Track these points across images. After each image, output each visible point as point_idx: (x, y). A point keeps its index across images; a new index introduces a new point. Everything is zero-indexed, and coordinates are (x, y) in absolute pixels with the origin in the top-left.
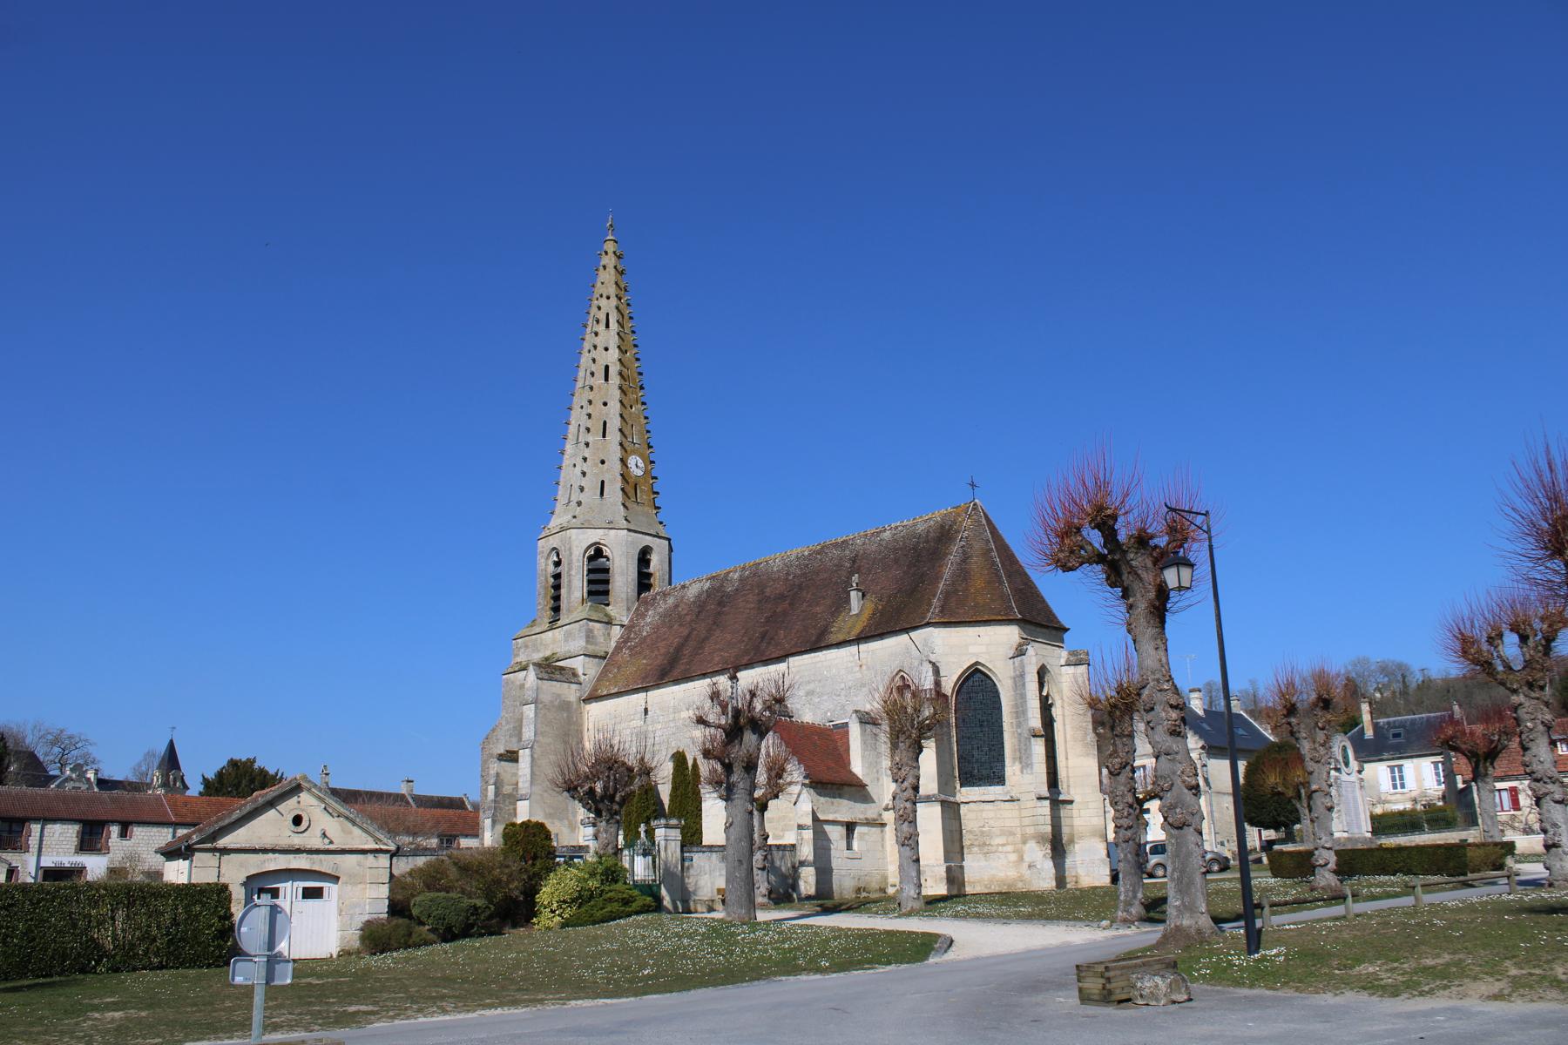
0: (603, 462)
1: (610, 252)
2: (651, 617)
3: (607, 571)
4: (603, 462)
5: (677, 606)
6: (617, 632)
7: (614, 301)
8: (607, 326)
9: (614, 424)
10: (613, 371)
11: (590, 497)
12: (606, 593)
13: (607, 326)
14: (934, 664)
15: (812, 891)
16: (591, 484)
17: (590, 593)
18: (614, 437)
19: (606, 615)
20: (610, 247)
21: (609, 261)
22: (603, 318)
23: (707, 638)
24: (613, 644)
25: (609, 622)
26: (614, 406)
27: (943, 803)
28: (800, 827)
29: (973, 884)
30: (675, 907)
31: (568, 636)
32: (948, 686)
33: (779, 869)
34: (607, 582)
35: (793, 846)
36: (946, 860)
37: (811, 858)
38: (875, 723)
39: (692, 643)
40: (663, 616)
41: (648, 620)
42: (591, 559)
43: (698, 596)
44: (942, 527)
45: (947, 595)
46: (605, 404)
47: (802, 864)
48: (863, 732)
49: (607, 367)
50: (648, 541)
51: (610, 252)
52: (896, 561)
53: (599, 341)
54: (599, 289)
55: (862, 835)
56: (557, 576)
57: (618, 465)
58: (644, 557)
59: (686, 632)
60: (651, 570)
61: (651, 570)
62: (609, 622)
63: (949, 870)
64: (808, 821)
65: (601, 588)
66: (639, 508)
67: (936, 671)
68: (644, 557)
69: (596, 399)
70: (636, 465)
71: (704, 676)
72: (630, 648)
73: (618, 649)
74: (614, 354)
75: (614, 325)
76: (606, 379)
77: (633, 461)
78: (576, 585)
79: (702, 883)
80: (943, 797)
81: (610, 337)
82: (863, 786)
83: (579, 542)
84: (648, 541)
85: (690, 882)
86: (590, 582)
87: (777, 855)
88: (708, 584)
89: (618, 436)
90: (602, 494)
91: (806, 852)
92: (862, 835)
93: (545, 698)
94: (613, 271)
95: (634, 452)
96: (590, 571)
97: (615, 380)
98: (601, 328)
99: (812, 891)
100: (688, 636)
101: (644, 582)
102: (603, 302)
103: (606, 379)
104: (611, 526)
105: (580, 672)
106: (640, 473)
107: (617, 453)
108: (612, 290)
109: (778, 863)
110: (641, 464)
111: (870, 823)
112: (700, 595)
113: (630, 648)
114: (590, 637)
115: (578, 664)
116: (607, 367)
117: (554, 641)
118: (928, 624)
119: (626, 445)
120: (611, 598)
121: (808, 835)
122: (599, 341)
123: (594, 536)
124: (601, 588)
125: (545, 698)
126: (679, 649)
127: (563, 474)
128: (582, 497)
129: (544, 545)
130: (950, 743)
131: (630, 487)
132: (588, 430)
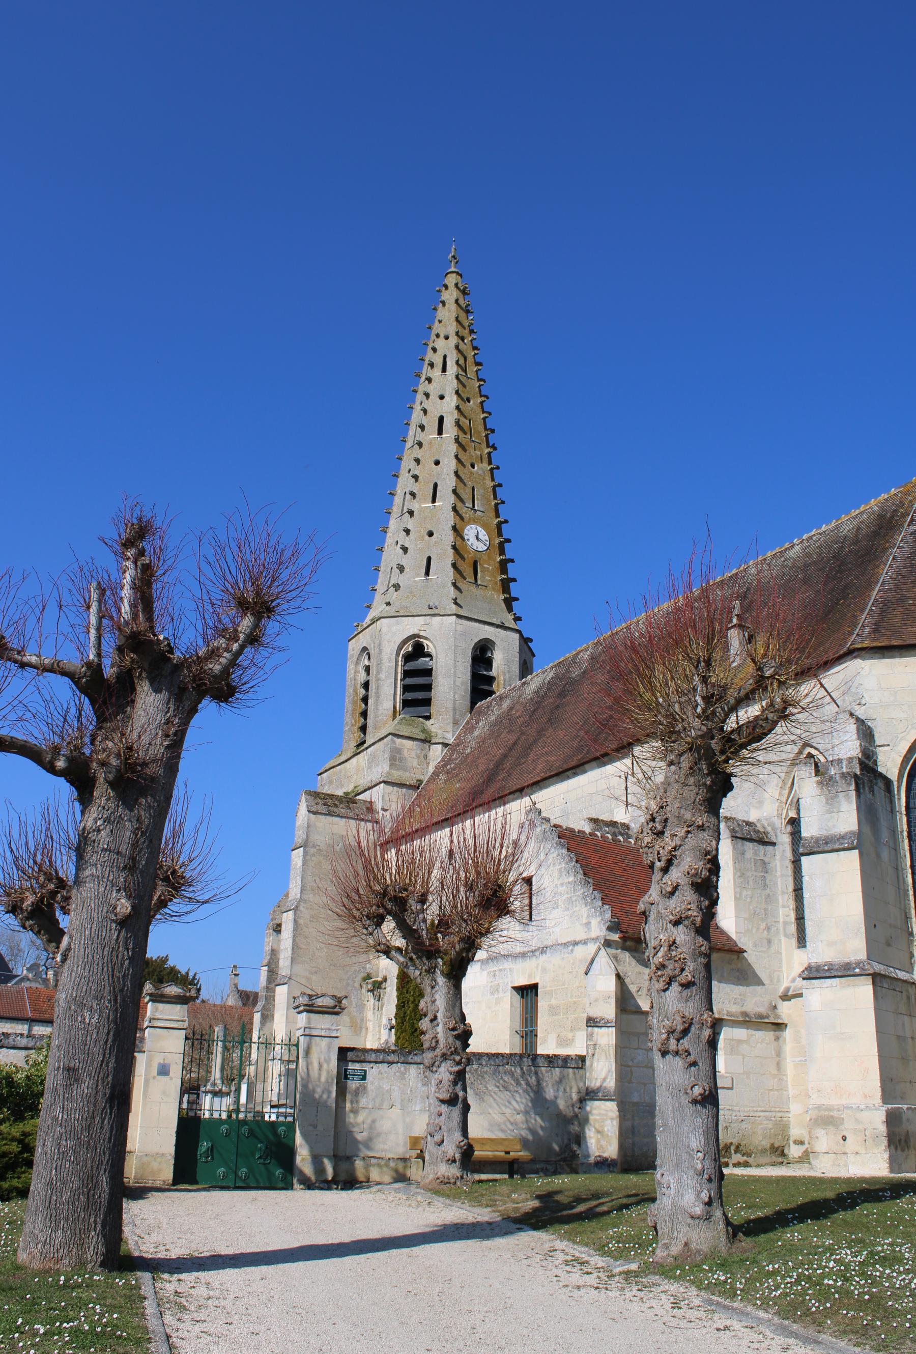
0: (431, 534)
1: (451, 285)
2: (482, 727)
3: (428, 672)
4: (431, 534)
5: (511, 709)
6: (437, 753)
7: (454, 340)
8: (444, 370)
9: (448, 483)
10: (449, 423)
11: (413, 577)
12: (427, 702)
13: (444, 370)
14: (860, 722)
15: (611, 1150)
16: (414, 562)
17: (406, 703)
18: (446, 500)
19: (424, 731)
20: (451, 280)
21: (450, 295)
22: (438, 361)
23: (536, 741)
24: (431, 769)
25: (427, 741)
26: (449, 464)
27: (876, 978)
28: (592, 1022)
29: (512, 1045)
30: (319, 1169)
31: (373, 760)
32: (890, 763)
33: (554, 1103)
34: (428, 688)
35: (582, 1059)
36: (886, 1097)
37: (611, 1083)
38: (764, 841)
39: (516, 752)
40: (492, 725)
41: (476, 733)
42: (408, 658)
43: (536, 693)
44: (881, 517)
45: (885, 607)
46: (437, 463)
47: (590, 1094)
48: (739, 856)
49: (441, 419)
50: (488, 632)
51: (451, 285)
52: (806, 581)
53: (431, 388)
54: (437, 328)
55: (734, 1046)
56: (366, 685)
57: (450, 537)
58: (482, 655)
59: (512, 738)
60: (494, 673)
61: (494, 673)
62: (427, 741)
63: (892, 1119)
64: (609, 1011)
65: (420, 695)
66: (479, 592)
67: (866, 733)
68: (482, 655)
69: (431, 455)
70: (477, 538)
71: (520, 791)
72: (448, 773)
73: (435, 774)
74: (452, 401)
75: (452, 369)
76: (440, 432)
77: (470, 532)
78: (387, 693)
79: (384, 1125)
80: (878, 968)
81: (446, 383)
82: (737, 952)
83: (388, 636)
84: (488, 632)
85: (359, 1121)
86: (406, 688)
87: (550, 1076)
88: (551, 674)
89: (452, 499)
90: (427, 573)
91: (603, 1071)
92: (729, 1040)
93: (320, 839)
94: (453, 307)
95: (474, 521)
96: (407, 674)
97: (450, 431)
98: (436, 373)
99: (611, 1150)
100: (515, 743)
101: (481, 686)
102: (440, 344)
103: (440, 432)
104: (433, 612)
105: (379, 806)
106: (481, 547)
107: (450, 519)
108: (452, 328)
109: (550, 1093)
110: (483, 535)
111: (748, 1021)
112: (540, 688)
113: (448, 773)
114: (396, 759)
115: (377, 796)
116: (441, 419)
117: (358, 770)
118: (851, 653)
119: (463, 510)
120: (434, 709)
121: (607, 1037)
122: (431, 388)
123: (411, 626)
124: (420, 695)
125: (320, 839)
126: (499, 765)
127: (385, 555)
128: (402, 580)
129: (354, 647)
130: (898, 869)
131: (465, 566)
132: (413, 495)
